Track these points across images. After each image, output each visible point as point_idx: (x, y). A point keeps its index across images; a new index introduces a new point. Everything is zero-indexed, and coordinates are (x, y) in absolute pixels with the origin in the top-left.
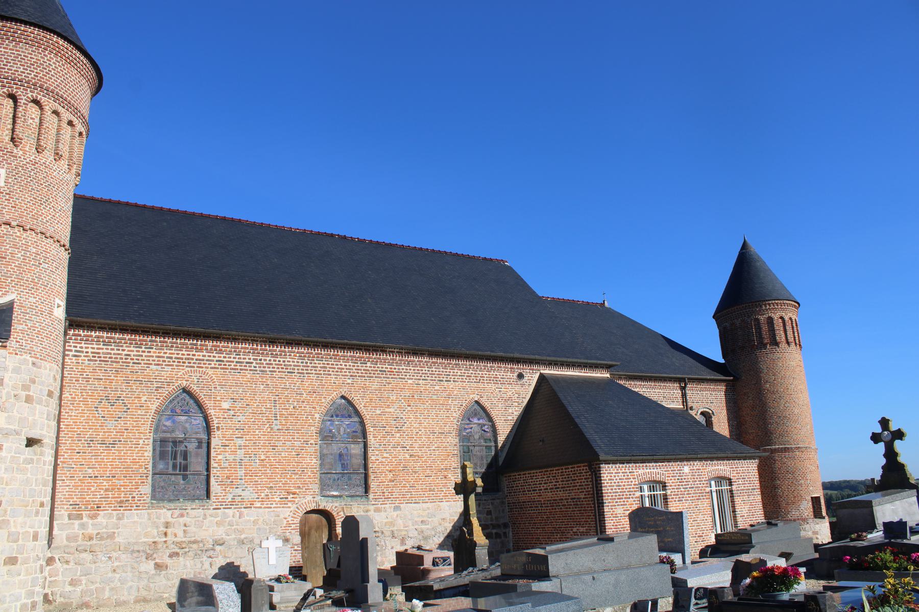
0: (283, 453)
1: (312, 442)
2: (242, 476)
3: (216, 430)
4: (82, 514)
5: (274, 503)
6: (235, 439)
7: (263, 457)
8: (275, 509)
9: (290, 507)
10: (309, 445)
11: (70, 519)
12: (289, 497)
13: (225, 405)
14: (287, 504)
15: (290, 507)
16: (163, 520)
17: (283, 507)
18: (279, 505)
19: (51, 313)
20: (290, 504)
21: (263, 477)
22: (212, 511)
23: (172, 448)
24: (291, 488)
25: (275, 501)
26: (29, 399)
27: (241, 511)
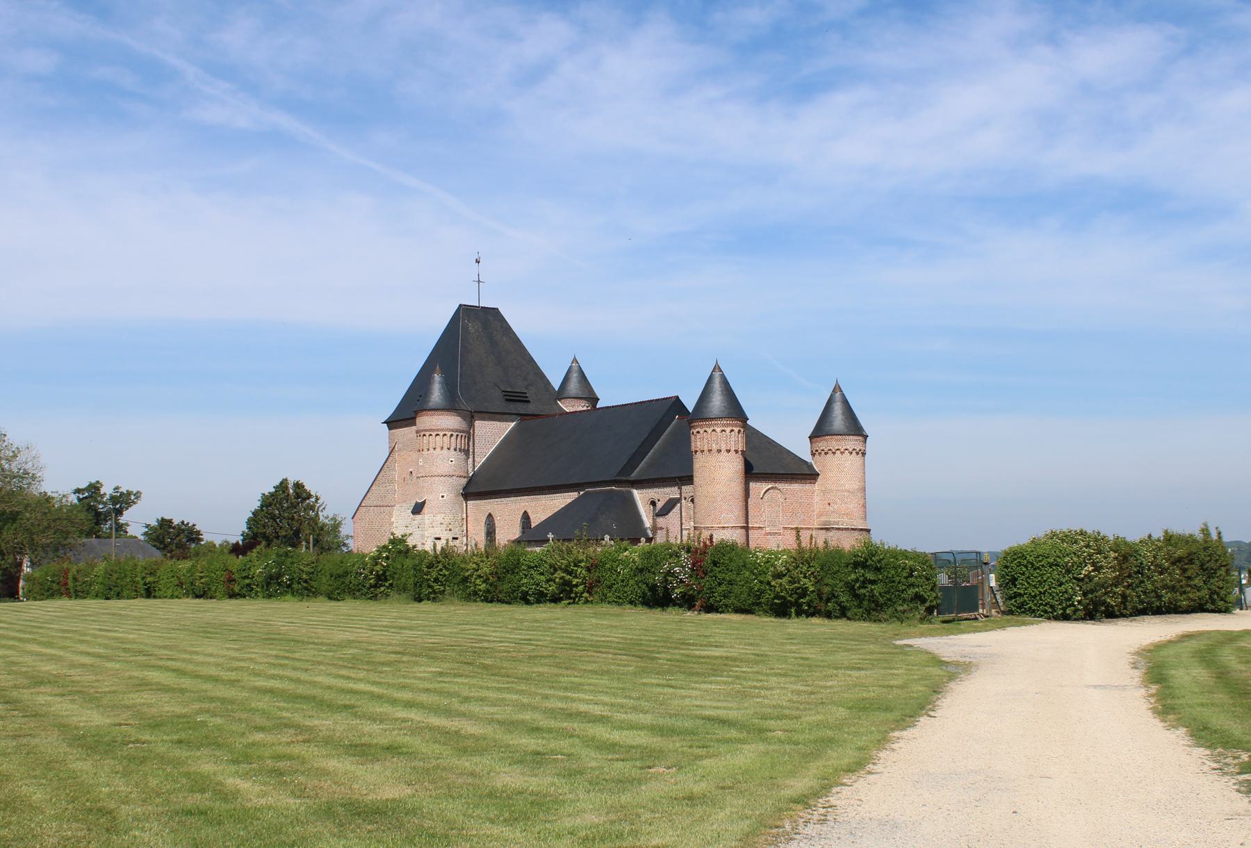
13: (498, 518)
19: (438, 499)
26: (433, 527)
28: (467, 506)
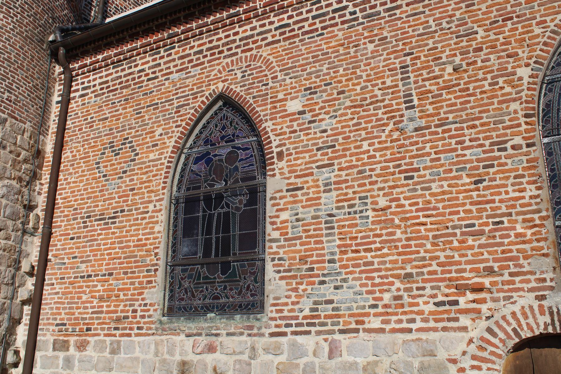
0: (433, 185)
1: (518, 140)
2: (332, 254)
3: (275, 160)
4: (67, 341)
5: (418, 318)
6: (315, 171)
7: (382, 202)
8: (423, 336)
9: (464, 329)
10: (510, 151)
11: (54, 349)
12: (462, 300)
13: (294, 106)
14: (456, 320)
15: (464, 329)
16: (178, 358)
17: (445, 329)
18: (432, 324)
20: (464, 321)
21: (385, 251)
22: (267, 340)
23: (204, 211)
24: (466, 275)
25: (420, 313)
27: (333, 341)
28: (66, 102)
